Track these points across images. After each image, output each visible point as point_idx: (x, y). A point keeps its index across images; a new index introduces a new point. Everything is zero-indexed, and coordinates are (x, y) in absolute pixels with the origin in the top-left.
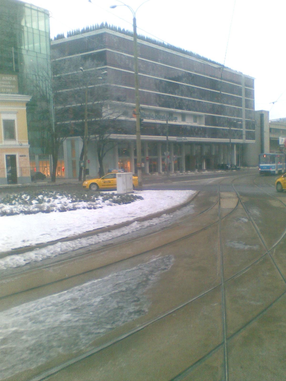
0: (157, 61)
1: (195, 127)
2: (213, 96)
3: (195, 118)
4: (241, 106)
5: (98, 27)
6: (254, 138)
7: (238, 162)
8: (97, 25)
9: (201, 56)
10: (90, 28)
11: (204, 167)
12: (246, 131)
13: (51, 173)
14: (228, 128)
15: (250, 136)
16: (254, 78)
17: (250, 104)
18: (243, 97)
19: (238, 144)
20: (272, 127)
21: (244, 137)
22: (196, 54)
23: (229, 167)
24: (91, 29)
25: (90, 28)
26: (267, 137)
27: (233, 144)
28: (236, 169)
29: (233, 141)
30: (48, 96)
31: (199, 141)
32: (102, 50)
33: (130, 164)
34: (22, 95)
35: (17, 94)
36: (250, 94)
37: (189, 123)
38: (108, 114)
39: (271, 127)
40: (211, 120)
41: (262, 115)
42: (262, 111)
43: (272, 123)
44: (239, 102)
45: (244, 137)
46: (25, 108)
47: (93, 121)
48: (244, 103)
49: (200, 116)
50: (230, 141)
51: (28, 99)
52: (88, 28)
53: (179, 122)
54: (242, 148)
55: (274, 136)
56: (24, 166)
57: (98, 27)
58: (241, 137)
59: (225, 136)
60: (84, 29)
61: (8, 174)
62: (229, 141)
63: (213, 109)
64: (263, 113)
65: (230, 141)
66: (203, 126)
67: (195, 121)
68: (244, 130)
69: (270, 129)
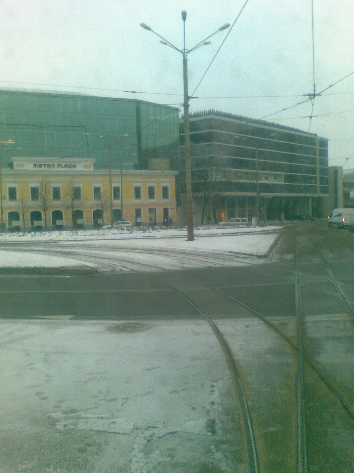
2: (291, 158)
3: (276, 177)
5: (206, 113)
6: (327, 192)
7: (313, 213)
8: (205, 111)
9: (281, 125)
10: (200, 112)
11: (283, 218)
13: (60, 254)
14: (306, 184)
15: (324, 190)
16: (327, 139)
17: (324, 162)
18: (318, 157)
19: (313, 198)
20: (347, 181)
21: (318, 191)
22: (277, 124)
23: (304, 217)
24: (201, 114)
25: (200, 112)
26: (341, 190)
27: (308, 198)
28: (311, 219)
29: (308, 195)
31: (242, 195)
34: (173, 171)
35: (170, 170)
36: (324, 153)
37: (271, 181)
38: (216, 177)
40: (289, 178)
41: (336, 170)
42: (336, 167)
43: (346, 177)
45: (318, 191)
46: (174, 179)
47: (10, 140)
48: (318, 162)
49: (281, 175)
50: (305, 195)
51: (176, 173)
52: (199, 113)
53: (263, 181)
54: (318, 201)
55: (346, 189)
56: (172, 213)
57: (206, 113)
58: (315, 192)
59: (300, 191)
60: (195, 112)
63: (291, 169)
64: (337, 169)
65: (305, 195)
67: (276, 179)
68: (318, 185)
69: (344, 184)
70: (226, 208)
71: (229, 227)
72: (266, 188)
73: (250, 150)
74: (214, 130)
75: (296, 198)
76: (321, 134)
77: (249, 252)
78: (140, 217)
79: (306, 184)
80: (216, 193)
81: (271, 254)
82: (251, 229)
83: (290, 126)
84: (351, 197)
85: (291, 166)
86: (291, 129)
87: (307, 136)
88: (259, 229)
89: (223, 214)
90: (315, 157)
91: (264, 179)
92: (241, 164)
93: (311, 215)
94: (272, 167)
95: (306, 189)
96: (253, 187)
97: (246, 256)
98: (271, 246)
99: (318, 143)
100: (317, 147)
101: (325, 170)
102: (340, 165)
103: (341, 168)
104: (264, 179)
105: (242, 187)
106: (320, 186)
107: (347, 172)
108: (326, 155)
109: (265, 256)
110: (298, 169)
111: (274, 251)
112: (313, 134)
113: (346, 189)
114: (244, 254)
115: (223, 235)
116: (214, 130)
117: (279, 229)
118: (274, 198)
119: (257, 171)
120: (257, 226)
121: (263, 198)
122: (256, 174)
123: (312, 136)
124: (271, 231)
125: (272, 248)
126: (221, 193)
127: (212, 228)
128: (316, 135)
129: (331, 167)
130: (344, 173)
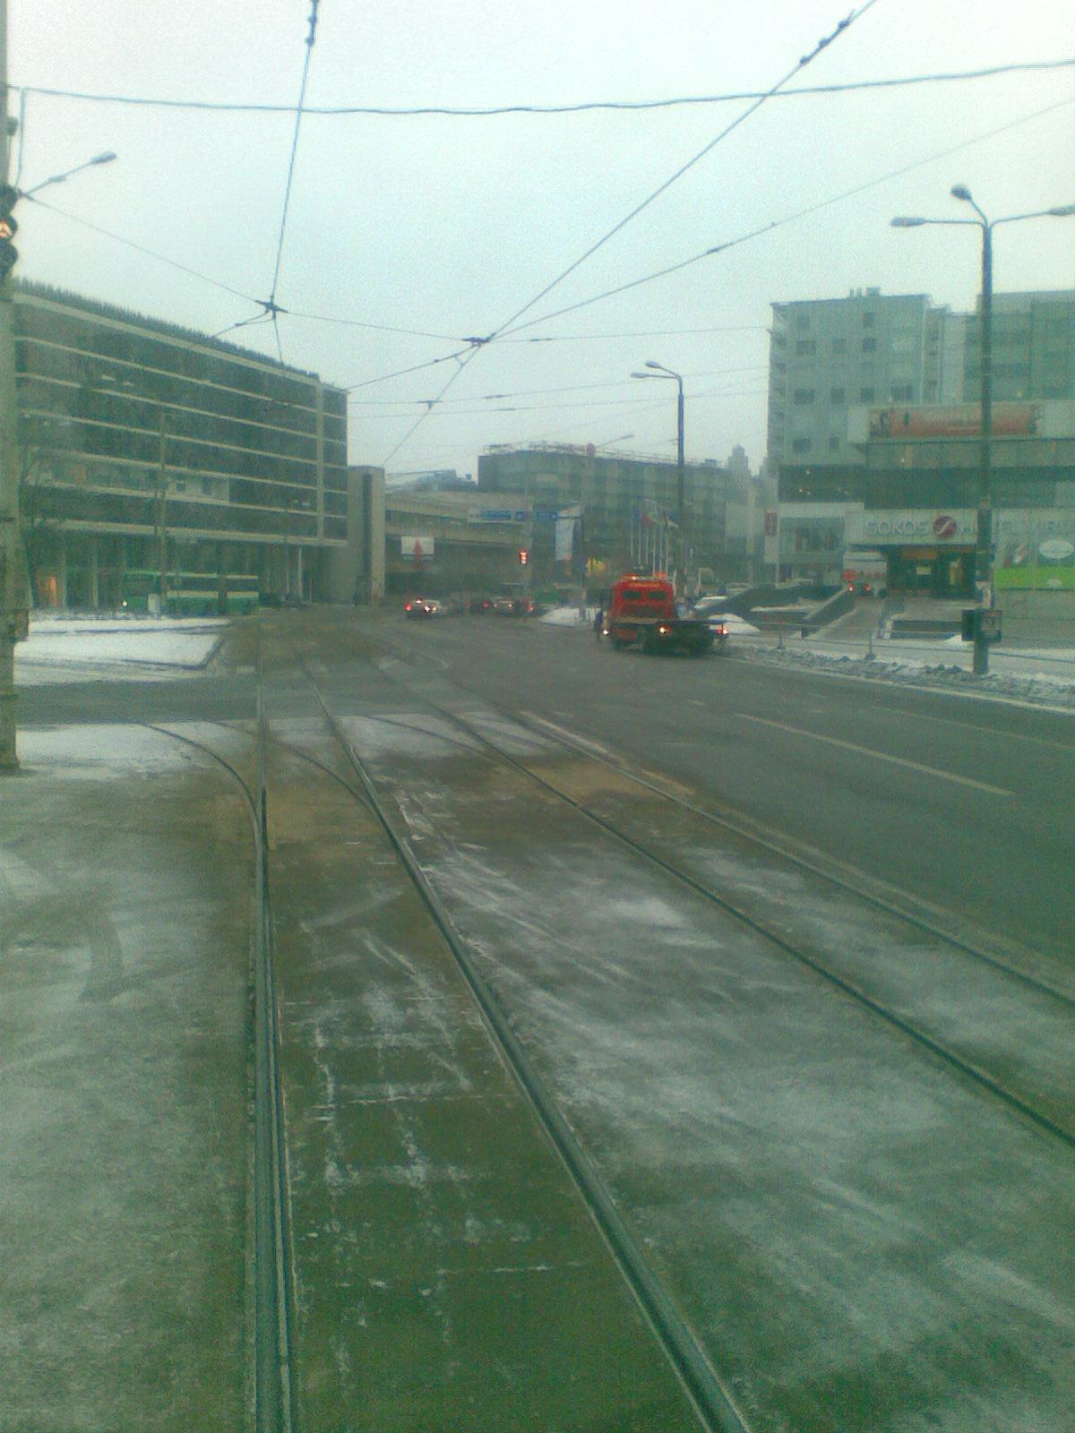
0: (126, 358)
1: (206, 507)
2: (247, 436)
3: (207, 484)
4: (314, 458)
7: (306, 591)
12: (325, 518)
15: (338, 530)
17: (336, 452)
18: (320, 438)
20: (392, 507)
21: (321, 529)
23: (283, 599)
29: (292, 540)
30: (936, 1008)
32: (287, 1375)
33: (57, 584)
36: (336, 429)
37: (192, 495)
39: (390, 508)
40: (242, 492)
41: (367, 477)
43: (402, 494)
44: (308, 449)
45: (321, 529)
48: (320, 453)
49: (221, 481)
53: (173, 495)
54: (318, 560)
58: (312, 532)
59: (274, 528)
61: (341, 442)
62: (153, 533)
63: (247, 465)
64: (370, 473)
66: (226, 503)
69: (389, 515)
70: (63, 563)
71: (90, 616)
72: (181, 515)
73: (134, 403)
74: (30, 339)
75: (261, 546)
76: (331, 376)
77: (166, 659)
78: (779, 500)
79: (289, 511)
80: (38, 520)
81: (210, 664)
82: (148, 623)
83: (247, 348)
84: (403, 552)
85: (249, 457)
86: (250, 355)
87: (282, 541)
88: (167, 622)
89: (53, 584)
90: (314, 436)
91: (173, 487)
92: (111, 443)
93: (301, 594)
94: (200, 458)
95: (294, 525)
96: (147, 511)
97: (162, 667)
98: (208, 654)
99: (320, 401)
100: (319, 411)
101: (338, 472)
102: (377, 464)
103: (381, 471)
104: (173, 487)
105: (114, 508)
106: (325, 518)
107: (400, 482)
108: (342, 435)
109: (202, 667)
110: (268, 467)
111: (215, 662)
112: (308, 373)
113: (392, 530)
114: (158, 664)
115: (80, 632)
116: (30, 339)
117: (220, 626)
118: (204, 542)
119: (163, 466)
120: (163, 617)
121: (171, 542)
122: (153, 475)
123: (309, 381)
124: (199, 630)
125: (211, 656)
126: (51, 521)
127: (44, 619)
128: (315, 376)
129: (354, 468)
130: (389, 482)
